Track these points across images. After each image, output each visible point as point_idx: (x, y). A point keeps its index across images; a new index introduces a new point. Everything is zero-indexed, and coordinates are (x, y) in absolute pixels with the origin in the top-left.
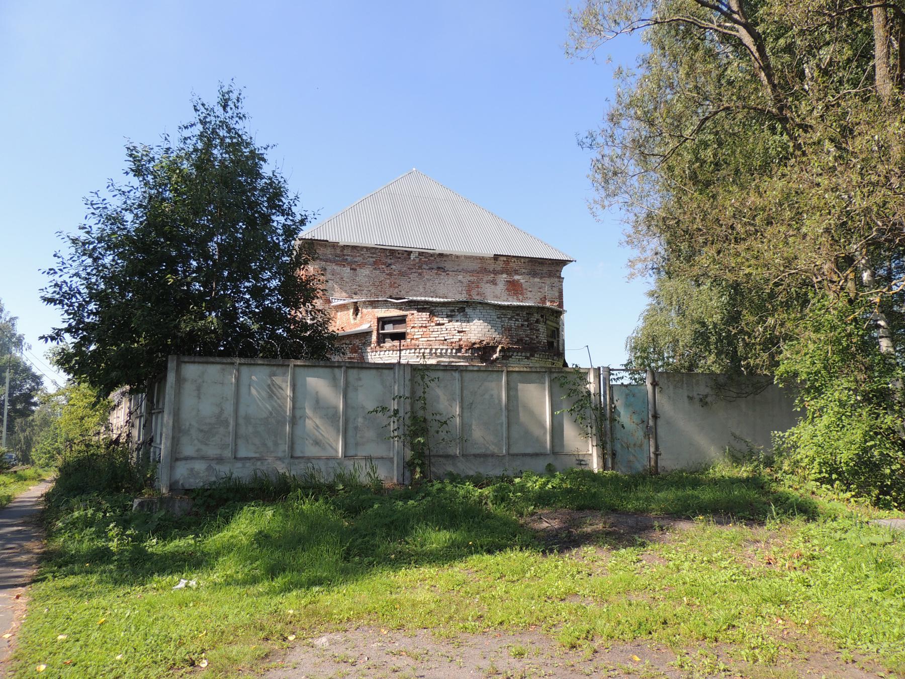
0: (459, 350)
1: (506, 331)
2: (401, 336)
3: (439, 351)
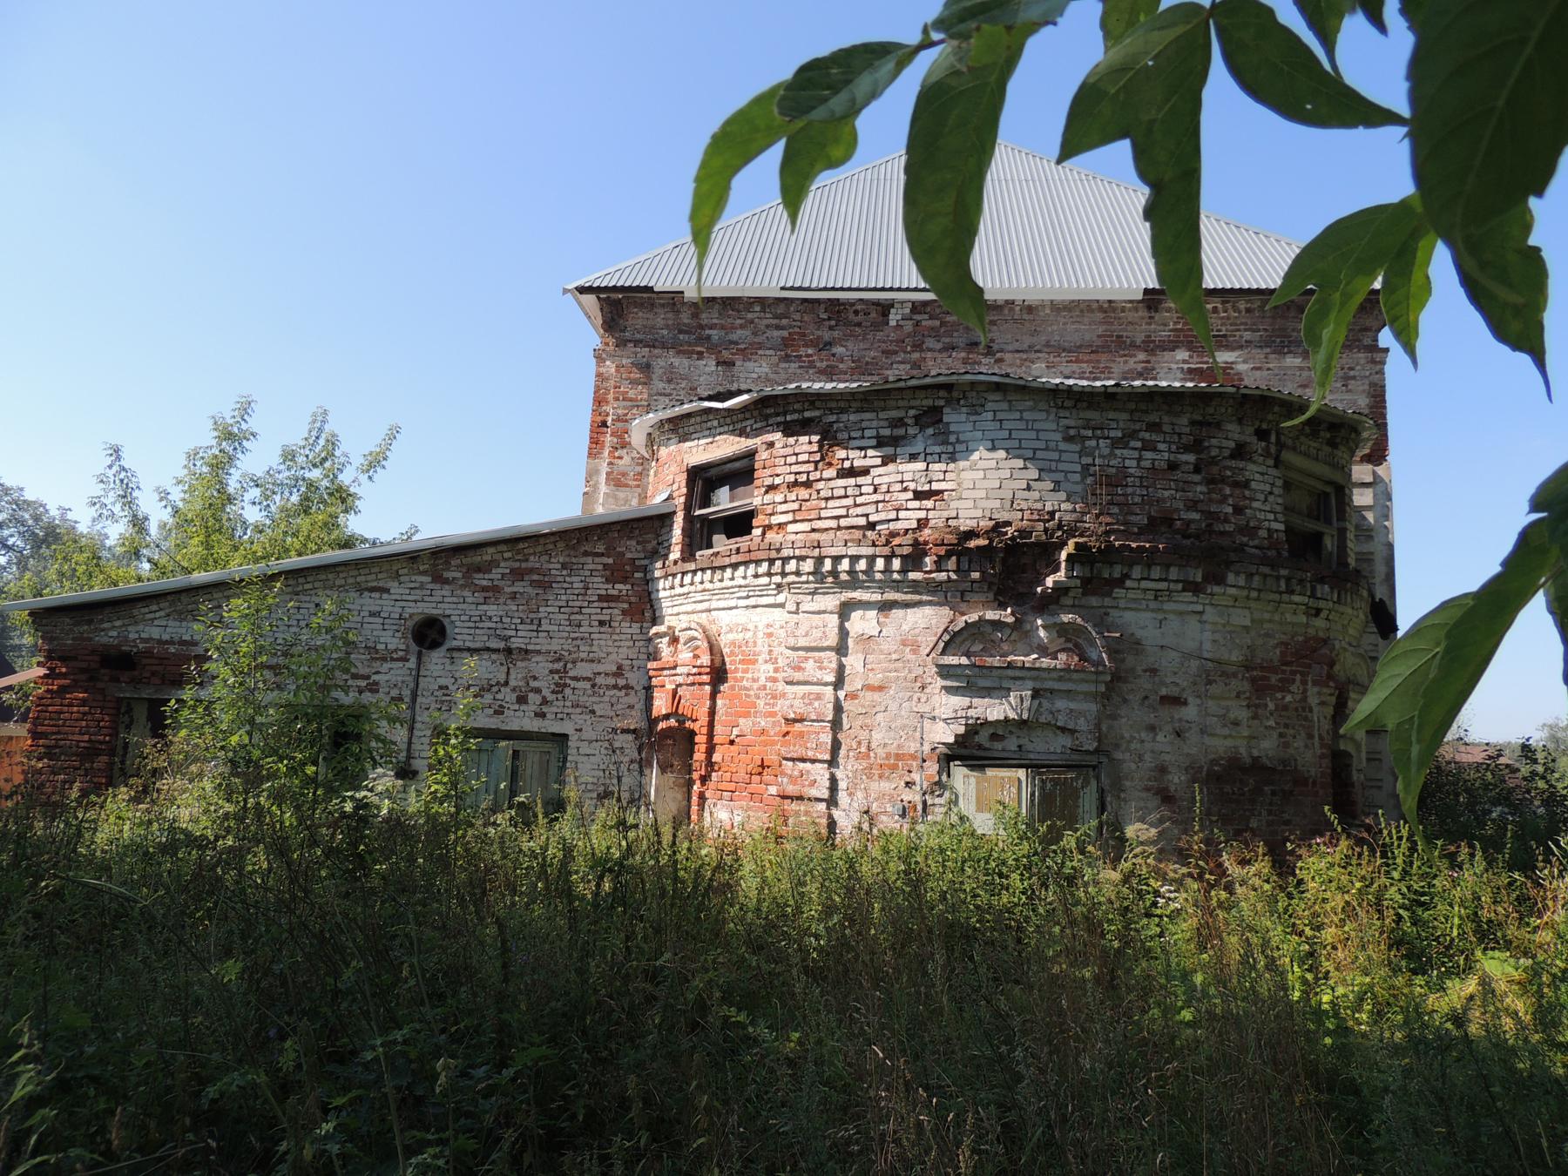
0: (914, 559)
1: (1106, 486)
2: (739, 524)
3: (845, 565)
